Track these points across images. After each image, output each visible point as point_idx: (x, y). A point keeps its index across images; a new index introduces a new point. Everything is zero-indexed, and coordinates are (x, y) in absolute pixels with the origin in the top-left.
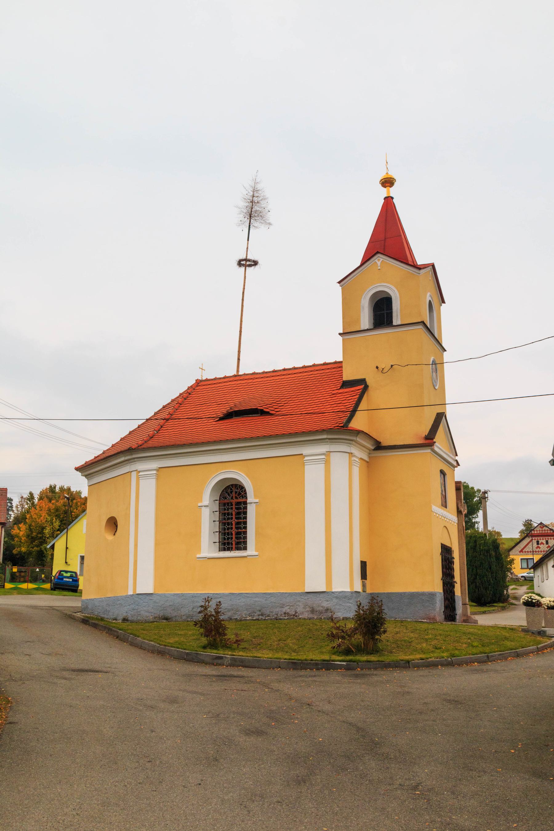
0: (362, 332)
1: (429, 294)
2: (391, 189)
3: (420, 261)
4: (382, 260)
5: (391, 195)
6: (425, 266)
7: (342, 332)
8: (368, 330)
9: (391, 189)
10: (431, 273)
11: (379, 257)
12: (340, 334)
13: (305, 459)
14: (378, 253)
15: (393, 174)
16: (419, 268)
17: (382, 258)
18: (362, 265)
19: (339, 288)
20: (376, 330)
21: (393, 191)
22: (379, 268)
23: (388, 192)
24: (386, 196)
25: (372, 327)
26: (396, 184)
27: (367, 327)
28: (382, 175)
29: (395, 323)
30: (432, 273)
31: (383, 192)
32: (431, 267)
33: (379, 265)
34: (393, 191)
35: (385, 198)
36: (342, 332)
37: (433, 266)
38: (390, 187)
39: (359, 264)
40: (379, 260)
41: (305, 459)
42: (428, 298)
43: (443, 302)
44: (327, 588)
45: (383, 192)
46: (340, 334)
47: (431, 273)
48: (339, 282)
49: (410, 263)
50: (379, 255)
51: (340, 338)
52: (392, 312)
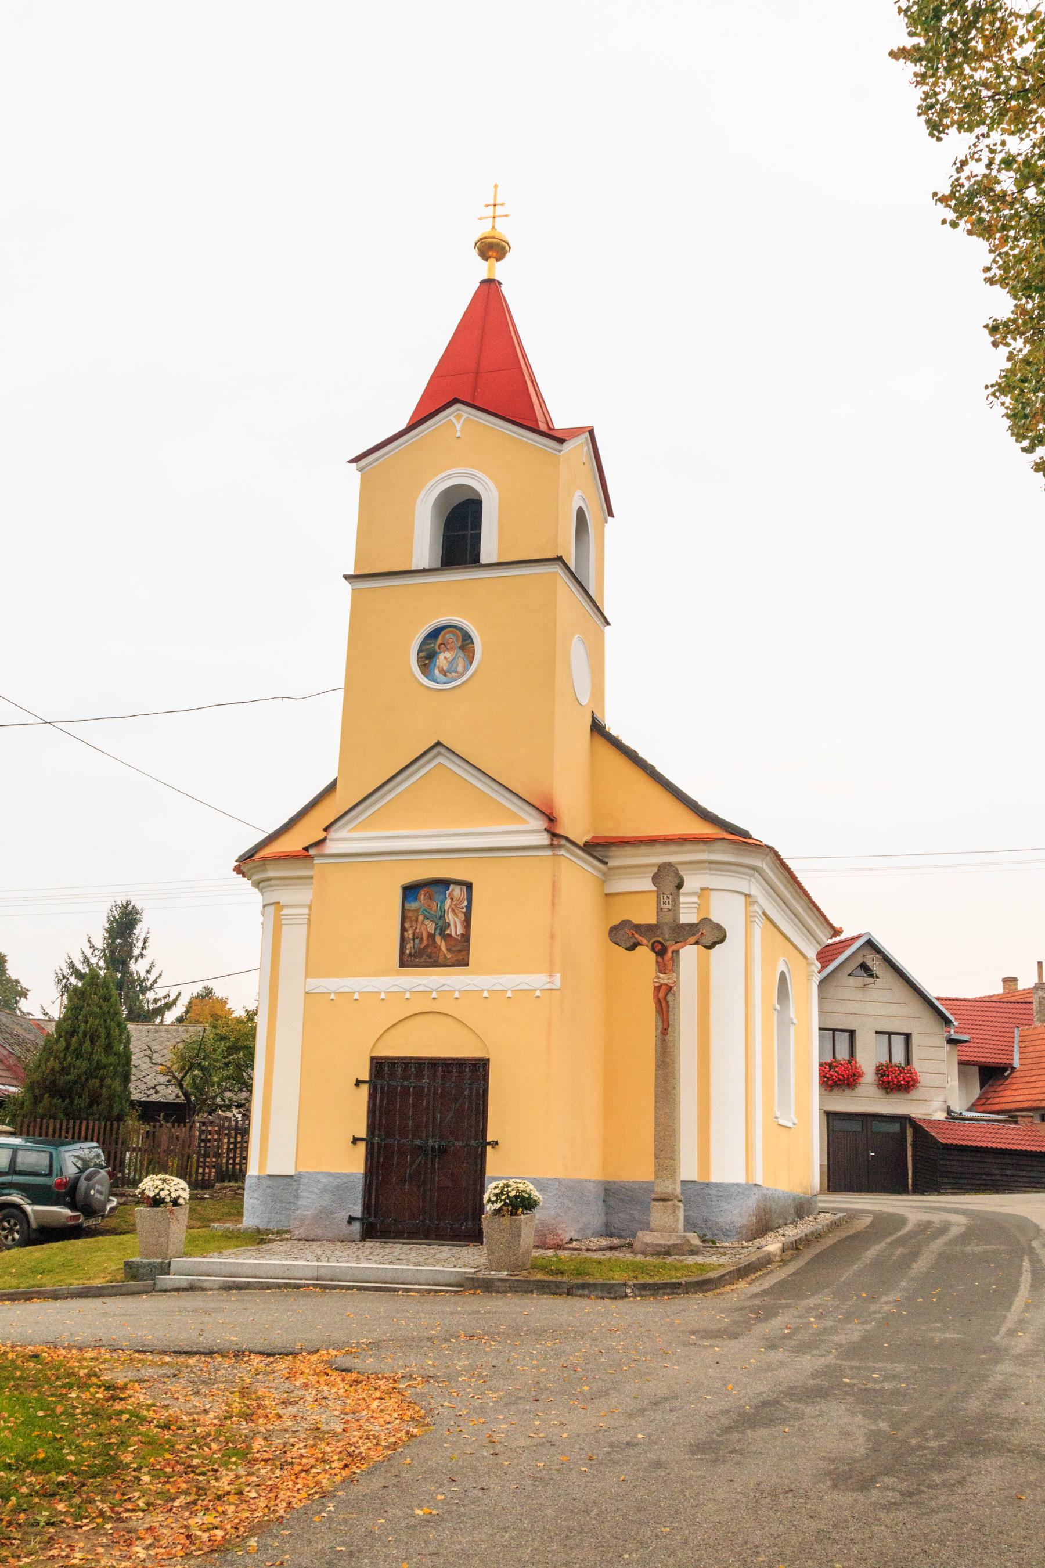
0: (417, 574)
1: (578, 493)
2: (499, 265)
3: (560, 422)
4: (465, 416)
5: (497, 278)
6: (574, 432)
7: (352, 573)
8: (424, 571)
9: (498, 265)
10: (587, 449)
11: (458, 410)
12: (346, 577)
13: (282, 913)
14: (455, 401)
15: (505, 230)
16: (560, 439)
17: (467, 413)
18: (411, 427)
19: (353, 475)
20: (468, 570)
21: (501, 271)
22: (458, 434)
23: (491, 269)
24: (485, 277)
25: (438, 565)
26: (508, 256)
27: (425, 564)
28: (483, 229)
29: (484, 560)
30: (589, 449)
31: (481, 270)
32: (587, 435)
33: (458, 429)
34: (501, 271)
35: (484, 282)
36: (351, 572)
37: (591, 432)
38: (498, 260)
39: (403, 426)
40: (458, 417)
41: (282, 913)
42: (576, 503)
43: (611, 513)
44: (259, 1172)
45: (481, 270)
46: (346, 577)
47: (585, 449)
48: (355, 460)
49: (543, 427)
50: (458, 406)
51: (347, 587)
52: (480, 534)
